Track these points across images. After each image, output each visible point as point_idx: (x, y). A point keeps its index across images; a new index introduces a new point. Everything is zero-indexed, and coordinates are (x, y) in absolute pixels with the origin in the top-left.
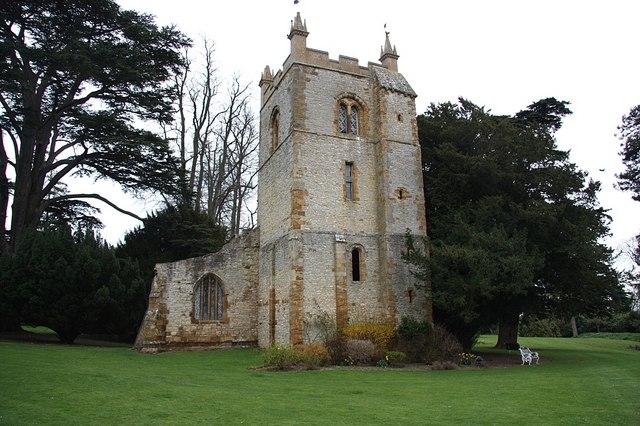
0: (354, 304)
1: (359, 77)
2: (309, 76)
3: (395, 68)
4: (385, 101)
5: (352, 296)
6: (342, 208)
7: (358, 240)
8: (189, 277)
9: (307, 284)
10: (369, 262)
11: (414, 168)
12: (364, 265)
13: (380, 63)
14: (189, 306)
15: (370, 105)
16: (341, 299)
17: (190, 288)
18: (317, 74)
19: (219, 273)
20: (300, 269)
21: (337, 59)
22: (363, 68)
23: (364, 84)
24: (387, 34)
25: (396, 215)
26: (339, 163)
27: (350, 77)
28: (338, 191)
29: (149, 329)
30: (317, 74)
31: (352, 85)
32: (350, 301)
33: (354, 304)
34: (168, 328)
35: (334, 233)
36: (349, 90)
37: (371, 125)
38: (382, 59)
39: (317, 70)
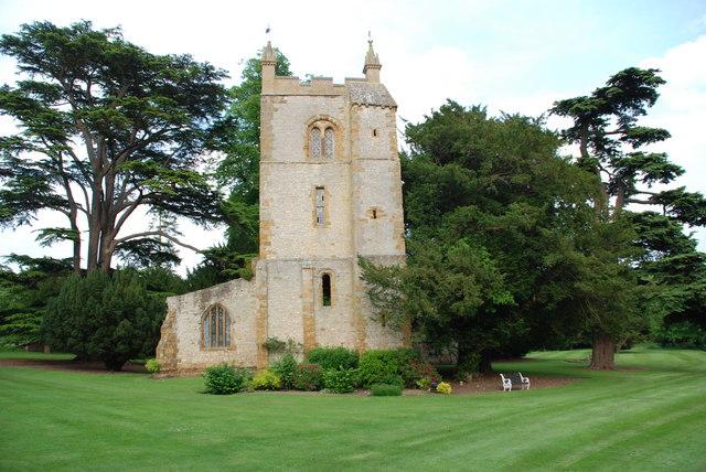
0: (323, 329)
1: (332, 96)
2: (275, 106)
3: (377, 79)
4: (358, 118)
5: (319, 320)
6: (310, 232)
7: (327, 265)
8: (197, 308)
9: (271, 311)
10: (339, 287)
11: (391, 184)
12: (173, 340)
13: (364, 76)
14: (198, 335)
15: (346, 125)
16: (309, 327)
17: (199, 318)
18: (285, 102)
19: (226, 303)
20: (265, 298)
21: (343, 82)
22: (338, 86)
23: (339, 102)
24: (370, 42)
25: (366, 236)
26: (309, 188)
27: (323, 98)
28: (309, 218)
29: (161, 357)
30: (285, 102)
31: (323, 106)
32: (319, 326)
33: (323, 329)
34: (179, 356)
35: (300, 260)
36: (322, 112)
37: (345, 145)
38: (365, 71)
39: (285, 98)
